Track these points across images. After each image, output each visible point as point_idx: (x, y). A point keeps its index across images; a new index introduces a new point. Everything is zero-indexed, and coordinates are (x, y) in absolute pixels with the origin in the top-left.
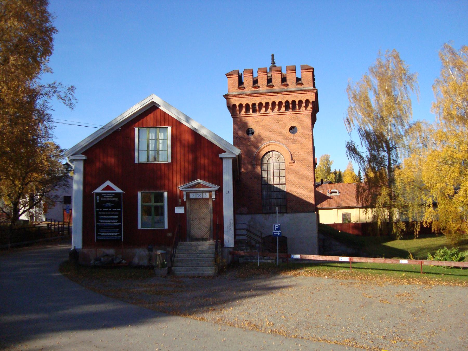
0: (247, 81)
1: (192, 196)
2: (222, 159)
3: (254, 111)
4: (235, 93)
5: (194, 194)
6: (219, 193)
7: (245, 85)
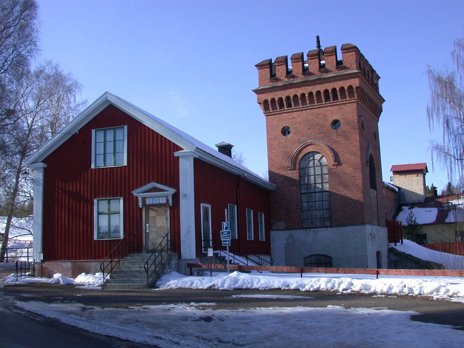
0: (280, 72)
1: (148, 202)
2: (178, 158)
3: (289, 105)
4: (266, 87)
5: (151, 199)
6: (176, 197)
7: (278, 75)
